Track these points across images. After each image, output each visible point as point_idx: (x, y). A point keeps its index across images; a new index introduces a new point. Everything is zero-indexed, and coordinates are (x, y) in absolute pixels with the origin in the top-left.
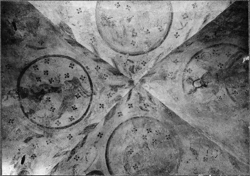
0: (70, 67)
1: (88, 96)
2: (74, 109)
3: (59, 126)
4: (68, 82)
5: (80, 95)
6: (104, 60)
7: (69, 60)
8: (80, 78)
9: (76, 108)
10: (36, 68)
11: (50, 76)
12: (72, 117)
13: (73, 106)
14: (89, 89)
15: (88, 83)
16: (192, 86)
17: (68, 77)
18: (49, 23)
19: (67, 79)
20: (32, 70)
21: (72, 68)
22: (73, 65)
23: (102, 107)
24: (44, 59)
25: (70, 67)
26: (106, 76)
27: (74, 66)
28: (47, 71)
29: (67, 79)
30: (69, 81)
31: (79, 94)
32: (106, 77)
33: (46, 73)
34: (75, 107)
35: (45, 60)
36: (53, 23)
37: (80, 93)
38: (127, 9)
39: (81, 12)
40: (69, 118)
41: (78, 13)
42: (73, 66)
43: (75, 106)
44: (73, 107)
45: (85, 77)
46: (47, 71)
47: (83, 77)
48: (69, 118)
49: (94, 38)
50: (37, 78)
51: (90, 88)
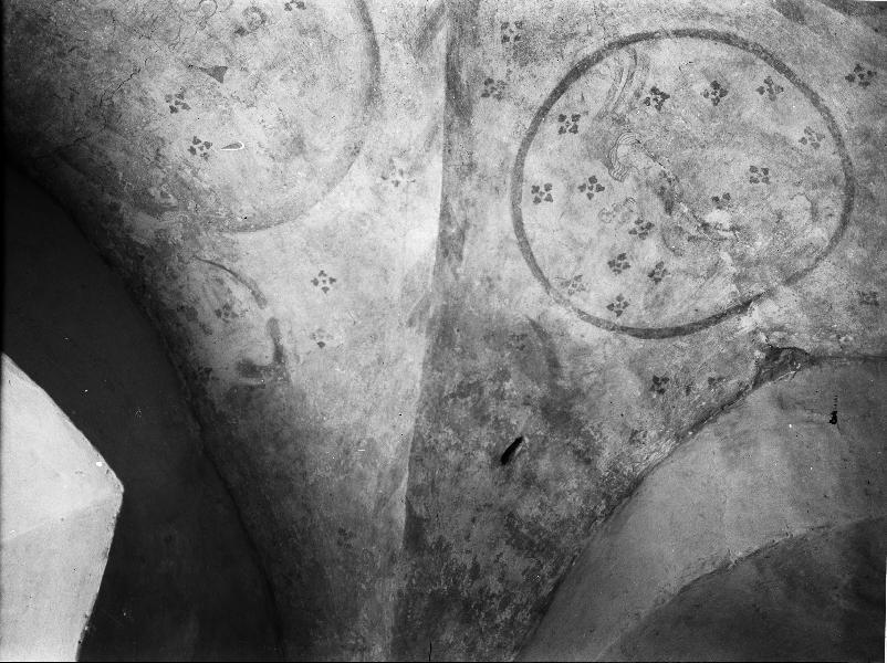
0: (549, 199)
1: (635, 58)
2: (724, 93)
3: (826, 132)
4: (616, 167)
5: (646, 94)
6: (444, 85)
7: (526, 219)
8: (575, 132)
9: (715, 85)
10: (618, 306)
11: (622, 241)
12: (761, 91)
13: (708, 102)
14: (608, 67)
15: (576, 89)
16: (515, 498)
17: (593, 180)
18: (434, 360)
19: (603, 176)
20: (636, 314)
21: (548, 187)
22: (536, 189)
23: (654, 103)
24: (573, 298)
25: (549, 199)
26: (507, 32)
27: (538, 184)
28: (611, 264)
29: (603, 176)
30: (609, 165)
31: (643, 98)
32: (513, 28)
33: (618, 264)
34: (711, 90)
35: (570, 293)
36: (428, 351)
37: (638, 95)
38: (185, 107)
39: (322, 273)
40: (773, 99)
41: (332, 280)
42: (542, 189)
43: (706, 96)
44: (716, 102)
45: (562, 118)
46: (611, 264)
47: (563, 124)
48: (773, 99)
49: (384, 178)
50: (657, 281)
51: (598, 66)
